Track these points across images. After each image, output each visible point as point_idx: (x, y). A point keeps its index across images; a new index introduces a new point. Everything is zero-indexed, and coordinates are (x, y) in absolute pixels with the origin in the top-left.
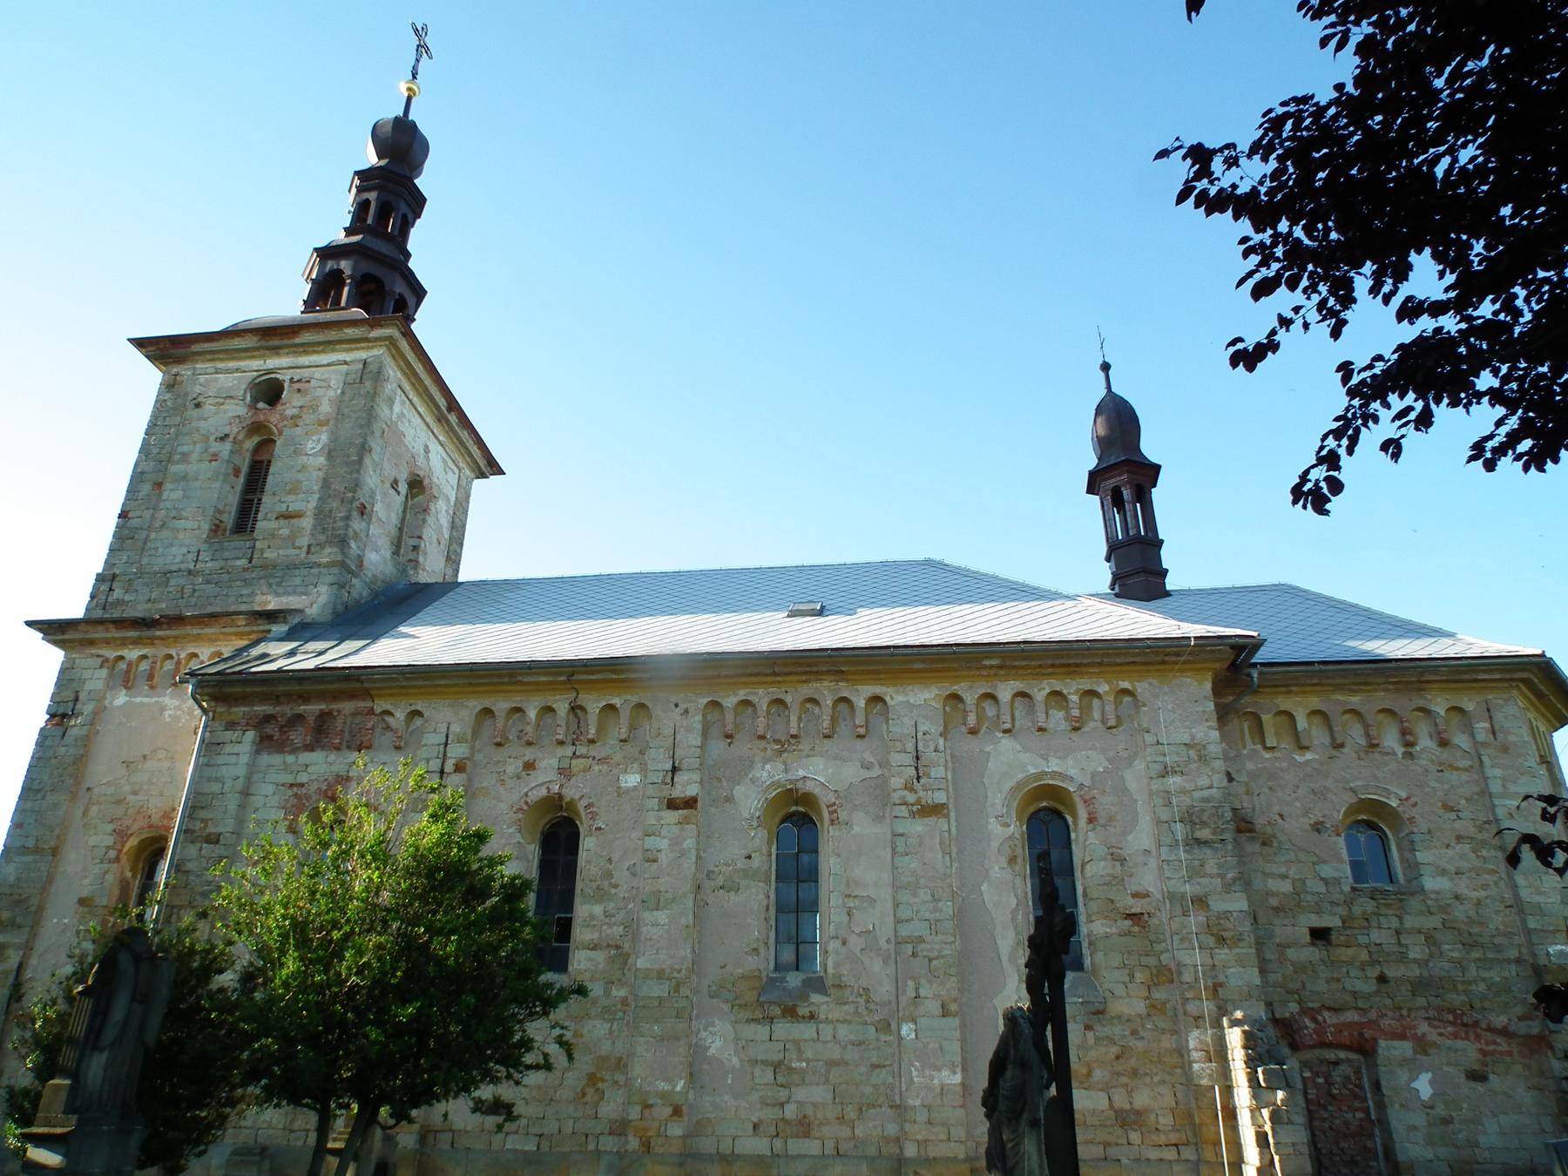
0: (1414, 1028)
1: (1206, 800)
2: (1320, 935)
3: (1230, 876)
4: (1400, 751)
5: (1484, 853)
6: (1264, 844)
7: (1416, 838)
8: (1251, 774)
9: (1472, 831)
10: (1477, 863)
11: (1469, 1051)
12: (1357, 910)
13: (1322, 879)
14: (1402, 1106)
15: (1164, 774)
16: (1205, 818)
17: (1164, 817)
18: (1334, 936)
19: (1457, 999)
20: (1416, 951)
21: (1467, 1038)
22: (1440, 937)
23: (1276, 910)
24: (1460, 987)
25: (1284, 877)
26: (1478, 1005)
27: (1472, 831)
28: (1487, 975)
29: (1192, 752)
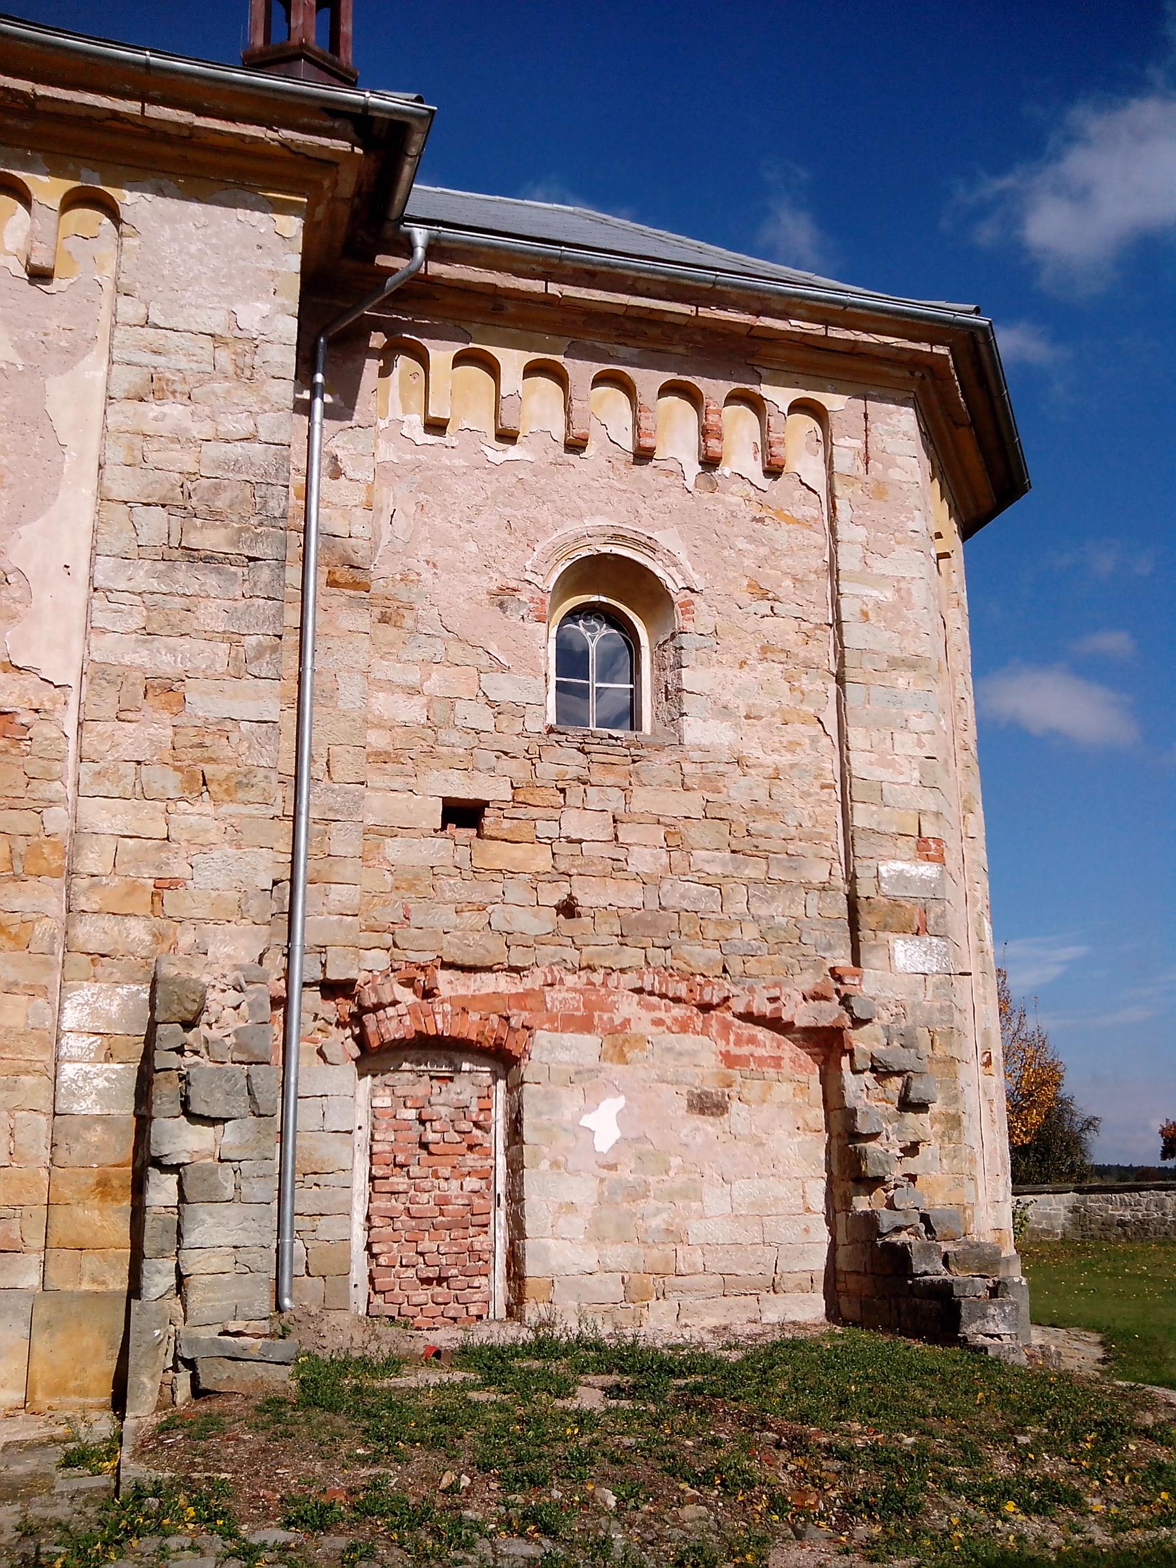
0: (612, 1008)
1: (236, 466)
2: (463, 814)
3: (251, 641)
4: (693, 468)
5: (805, 683)
6: (384, 619)
7: (684, 640)
8: (382, 470)
9: (792, 639)
10: (788, 699)
11: (701, 1054)
12: (547, 770)
13: (491, 704)
14: (555, 1164)
15: (154, 388)
16: (220, 504)
17: (119, 491)
18: (489, 821)
19: (700, 955)
20: (645, 858)
21: (704, 1032)
22: (695, 833)
23: (382, 758)
24: (711, 932)
25: (414, 691)
26: (736, 967)
27: (792, 639)
28: (763, 911)
29: (224, 357)
